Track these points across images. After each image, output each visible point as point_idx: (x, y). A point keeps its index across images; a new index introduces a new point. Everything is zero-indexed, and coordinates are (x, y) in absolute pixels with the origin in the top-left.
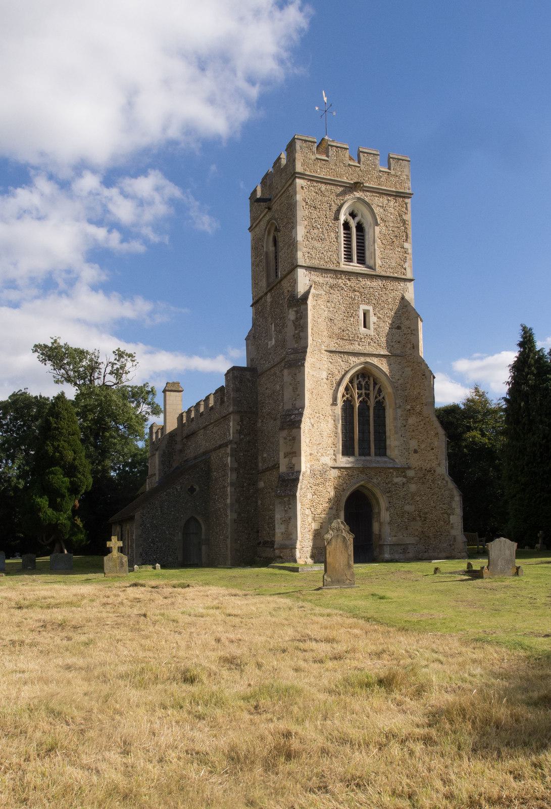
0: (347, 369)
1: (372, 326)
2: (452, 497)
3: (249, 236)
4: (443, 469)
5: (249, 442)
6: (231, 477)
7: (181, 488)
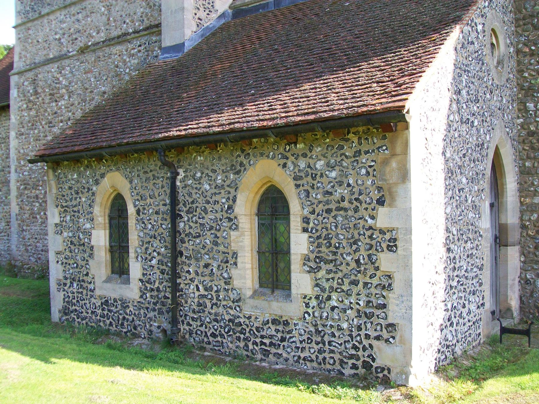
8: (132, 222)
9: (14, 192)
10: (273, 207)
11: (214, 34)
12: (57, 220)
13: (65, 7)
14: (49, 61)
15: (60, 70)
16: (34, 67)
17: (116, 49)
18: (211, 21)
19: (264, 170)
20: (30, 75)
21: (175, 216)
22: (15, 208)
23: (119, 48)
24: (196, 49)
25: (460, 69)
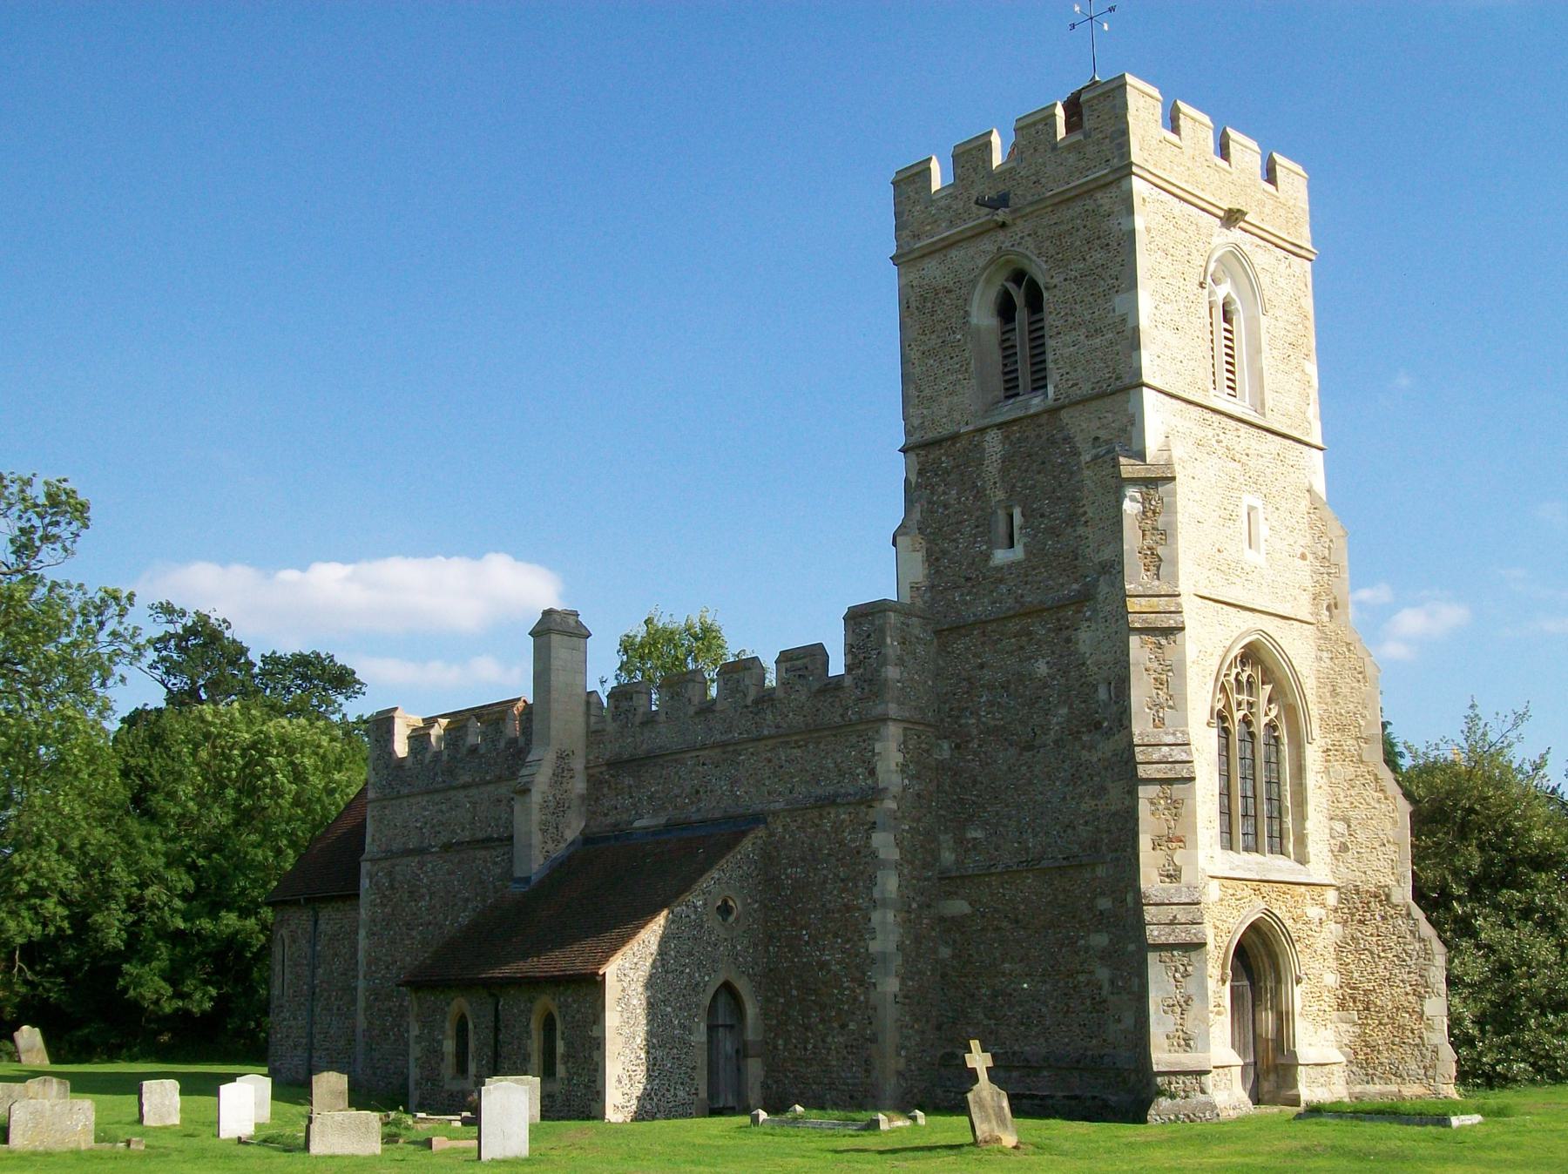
0: (1228, 643)
1: (1263, 545)
2: (1428, 955)
3: (889, 280)
4: (1403, 894)
5: (918, 795)
6: (890, 884)
7: (705, 904)
8: (471, 1034)
9: (361, 1003)
10: (549, 1025)
11: (561, 864)
12: (417, 1032)
13: (428, 792)
14: (408, 852)
15: (422, 865)
16: (389, 855)
17: (481, 854)
18: (559, 850)
19: (546, 1001)
20: (384, 864)
21: (497, 1030)
22: (361, 1022)
23: (483, 853)
24: (541, 882)
25: (664, 941)
